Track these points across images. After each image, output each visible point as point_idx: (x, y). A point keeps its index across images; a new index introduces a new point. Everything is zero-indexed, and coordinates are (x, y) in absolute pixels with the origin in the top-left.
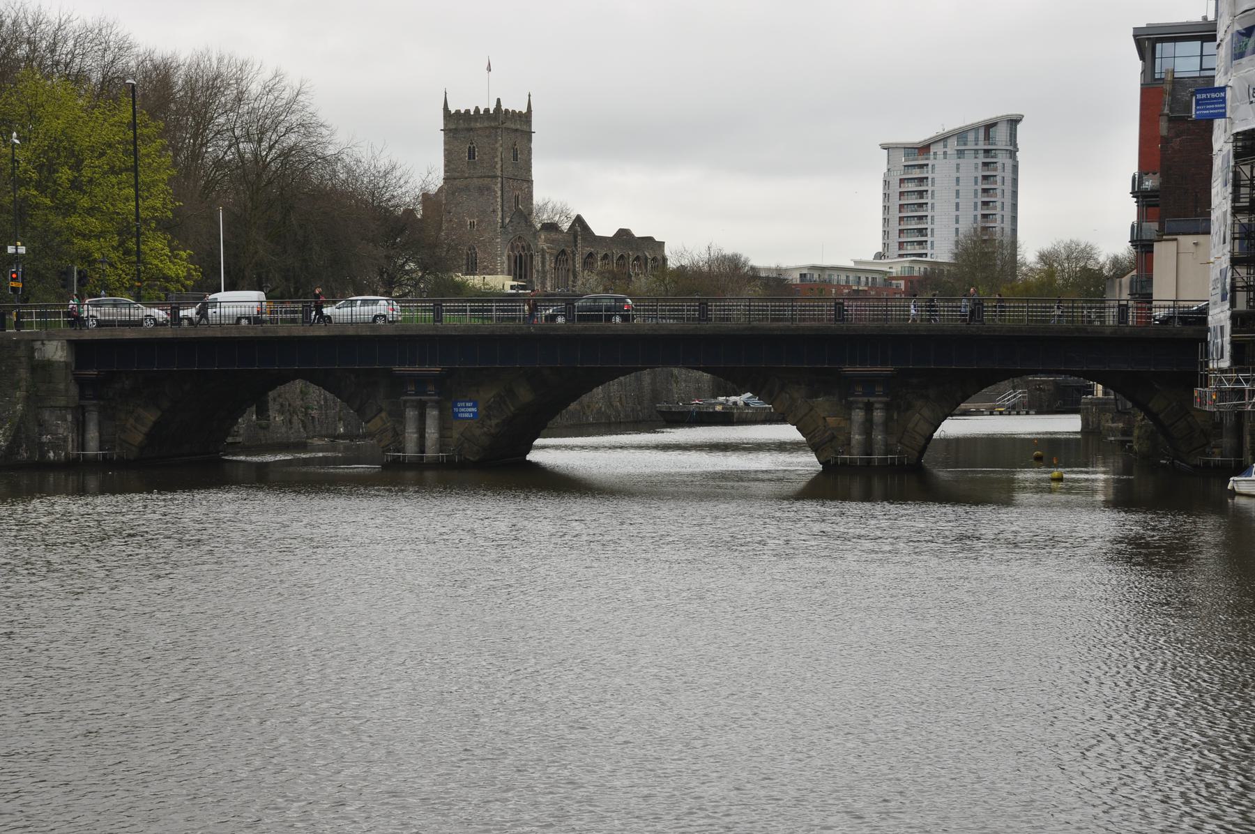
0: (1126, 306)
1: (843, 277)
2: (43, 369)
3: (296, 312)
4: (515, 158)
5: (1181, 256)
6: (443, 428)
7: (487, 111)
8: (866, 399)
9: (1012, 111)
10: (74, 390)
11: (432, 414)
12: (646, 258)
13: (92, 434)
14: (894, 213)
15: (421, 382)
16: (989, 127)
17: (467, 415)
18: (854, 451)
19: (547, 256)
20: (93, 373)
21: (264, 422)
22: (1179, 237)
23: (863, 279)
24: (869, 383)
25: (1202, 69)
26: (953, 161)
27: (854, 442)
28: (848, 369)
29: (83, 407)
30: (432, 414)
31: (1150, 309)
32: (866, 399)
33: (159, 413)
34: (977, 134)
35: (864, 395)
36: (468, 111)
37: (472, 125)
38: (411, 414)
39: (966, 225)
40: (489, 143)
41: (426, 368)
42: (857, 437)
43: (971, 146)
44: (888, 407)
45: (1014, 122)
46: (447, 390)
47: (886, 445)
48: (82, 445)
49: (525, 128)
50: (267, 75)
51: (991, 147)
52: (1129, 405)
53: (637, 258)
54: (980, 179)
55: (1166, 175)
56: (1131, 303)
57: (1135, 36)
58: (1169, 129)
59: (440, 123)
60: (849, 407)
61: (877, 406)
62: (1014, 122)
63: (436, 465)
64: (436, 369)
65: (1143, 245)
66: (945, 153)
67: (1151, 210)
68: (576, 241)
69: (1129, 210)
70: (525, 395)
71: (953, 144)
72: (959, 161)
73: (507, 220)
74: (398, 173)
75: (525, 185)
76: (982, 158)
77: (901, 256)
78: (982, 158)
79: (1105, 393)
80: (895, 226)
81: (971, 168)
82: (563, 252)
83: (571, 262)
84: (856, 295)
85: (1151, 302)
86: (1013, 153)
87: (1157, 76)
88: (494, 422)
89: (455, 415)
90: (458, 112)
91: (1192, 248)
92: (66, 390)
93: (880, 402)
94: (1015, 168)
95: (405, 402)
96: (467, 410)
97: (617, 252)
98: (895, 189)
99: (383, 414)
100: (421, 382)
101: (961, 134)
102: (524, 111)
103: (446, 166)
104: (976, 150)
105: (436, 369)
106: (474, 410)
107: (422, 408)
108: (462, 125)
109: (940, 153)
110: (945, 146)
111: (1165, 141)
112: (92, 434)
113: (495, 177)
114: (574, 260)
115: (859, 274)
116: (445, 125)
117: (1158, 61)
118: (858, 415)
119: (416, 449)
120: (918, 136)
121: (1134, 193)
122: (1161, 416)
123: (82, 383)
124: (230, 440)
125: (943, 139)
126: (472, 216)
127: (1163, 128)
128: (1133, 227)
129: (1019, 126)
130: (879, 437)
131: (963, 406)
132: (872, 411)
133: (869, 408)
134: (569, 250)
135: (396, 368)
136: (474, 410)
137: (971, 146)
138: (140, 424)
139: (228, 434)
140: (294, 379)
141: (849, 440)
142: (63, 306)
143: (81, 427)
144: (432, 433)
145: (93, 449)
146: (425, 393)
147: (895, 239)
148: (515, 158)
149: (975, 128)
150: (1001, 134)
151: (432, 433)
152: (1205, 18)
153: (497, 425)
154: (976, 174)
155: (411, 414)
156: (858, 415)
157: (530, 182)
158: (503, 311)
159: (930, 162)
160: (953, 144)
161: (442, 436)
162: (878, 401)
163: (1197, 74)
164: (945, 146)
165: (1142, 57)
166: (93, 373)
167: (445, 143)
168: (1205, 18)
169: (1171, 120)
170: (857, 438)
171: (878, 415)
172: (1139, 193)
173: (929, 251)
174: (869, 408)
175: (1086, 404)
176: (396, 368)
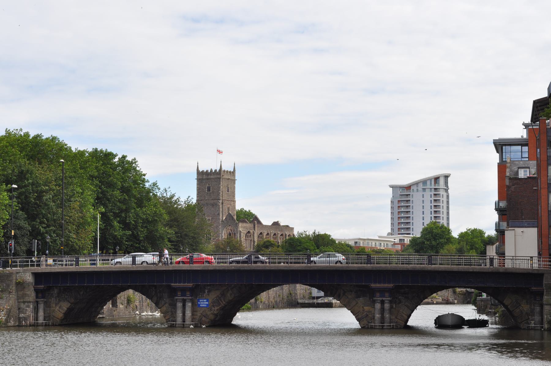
0: (493, 258)
1: (374, 243)
2: (20, 285)
4: (228, 191)
6: (193, 312)
7: (216, 171)
8: (381, 299)
9: (446, 172)
10: (33, 294)
11: (189, 305)
12: (286, 235)
13: (41, 314)
14: (396, 210)
15: (183, 291)
16: (437, 179)
17: (204, 305)
18: (376, 322)
19: (242, 234)
20: (42, 287)
21: (114, 309)
22: (516, 229)
23: (382, 244)
24: (382, 291)
26: (421, 193)
27: (376, 318)
28: (373, 285)
29: (37, 302)
30: (189, 305)
31: (504, 260)
32: (381, 299)
33: (69, 304)
35: (380, 297)
36: (207, 171)
37: (209, 177)
38: (179, 305)
39: (427, 221)
40: (213, 183)
41: (186, 284)
42: (377, 315)
43: (428, 186)
44: (391, 302)
45: (446, 177)
46: (195, 293)
47: (390, 319)
48: (36, 318)
49: (232, 178)
50: (151, 182)
51: (437, 185)
52: (497, 302)
53: (282, 235)
54: (433, 201)
55: (509, 200)
56: (497, 257)
57: (494, 143)
58: (510, 182)
59: (195, 176)
60: (374, 302)
61: (386, 302)
62: (446, 177)
63: (42, 325)
64: (190, 285)
65: (501, 232)
66: (417, 189)
67: (503, 216)
68: (254, 227)
69: (495, 217)
70: (230, 296)
71: (421, 186)
72: (424, 193)
73: (224, 218)
74: (175, 198)
75: (232, 203)
76: (433, 192)
77: (399, 234)
78: (433, 192)
79: (487, 296)
80: (396, 221)
81: (428, 196)
82: (249, 232)
83: (252, 236)
84: (379, 252)
85: (504, 257)
86: (446, 190)
87: (504, 160)
88: (216, 308)
90: (203, 171)
91: (521, 233)
92: (31, 294)
93: (388, 300)
94: (448, 197)
95: (177, 299)
96: (204, 303)
97: (272, 232)
98: (396, 205)
99: (167, 305)
100: (183, 291)
101: (424, 182)
102: (232, 170)
103: (197, 194)
104: (431, 189)
105: (190, 285)
106: (207, 303)
108: (205, 177)
109: (415, 190)
110: (417, 186)
111: (508, 187)
112: (41, 314)
113: (220, 200)
114: (254, 235)
116: (197, 177)
117: (504, 154)
118: (378, 306)
119: (181, 320)
120: (405, 181)
121: (496, 209)
122: (509, 307)
123: (37, 291)
124: (101, 316)
125: (417, 183)
126: (208, 216)
127: (507, 182)
128: (496, 224)
129: (449, 179)
130: (387, 316)
131: (426, 300)
132: (384, 304)
133: (382, 302)
134: (251, 231)
135: (173, 284)
136: (207, 303)
137: (428, 186)
138: (60, 309)
139: (99, 313)
140: (128, 289)
141: (374, 316)
142: (30, 258)
143: (36, 310)
144: (188, 313)
145: (41, 320)
146: (185, 296)
147: (396, 227)
148: (228, 191)
149: (430, 179)
150: (442, 181)
151: (188, 313)
152: (522, 136)
153: (217, 310)
154: (431, 199)
155: (179, 305)
156: (378, 306)
157: (234, 201)
158: (220, 259)
159: (411, 194)
160: (421, 186)
161: (193, 315)
162: (387, 299)
163: (520, 160)
164: (417, 186)
165: (498, 152)
166: (42, 287)
167: (198, 184)
168: (522, 136)
169: (510, 179)
170: (378, 316)
171: (387, 306)
172: (499, 210)
173: (411, 232)
174: (382, 302)
175: (479, 301)
176: (173, 284)
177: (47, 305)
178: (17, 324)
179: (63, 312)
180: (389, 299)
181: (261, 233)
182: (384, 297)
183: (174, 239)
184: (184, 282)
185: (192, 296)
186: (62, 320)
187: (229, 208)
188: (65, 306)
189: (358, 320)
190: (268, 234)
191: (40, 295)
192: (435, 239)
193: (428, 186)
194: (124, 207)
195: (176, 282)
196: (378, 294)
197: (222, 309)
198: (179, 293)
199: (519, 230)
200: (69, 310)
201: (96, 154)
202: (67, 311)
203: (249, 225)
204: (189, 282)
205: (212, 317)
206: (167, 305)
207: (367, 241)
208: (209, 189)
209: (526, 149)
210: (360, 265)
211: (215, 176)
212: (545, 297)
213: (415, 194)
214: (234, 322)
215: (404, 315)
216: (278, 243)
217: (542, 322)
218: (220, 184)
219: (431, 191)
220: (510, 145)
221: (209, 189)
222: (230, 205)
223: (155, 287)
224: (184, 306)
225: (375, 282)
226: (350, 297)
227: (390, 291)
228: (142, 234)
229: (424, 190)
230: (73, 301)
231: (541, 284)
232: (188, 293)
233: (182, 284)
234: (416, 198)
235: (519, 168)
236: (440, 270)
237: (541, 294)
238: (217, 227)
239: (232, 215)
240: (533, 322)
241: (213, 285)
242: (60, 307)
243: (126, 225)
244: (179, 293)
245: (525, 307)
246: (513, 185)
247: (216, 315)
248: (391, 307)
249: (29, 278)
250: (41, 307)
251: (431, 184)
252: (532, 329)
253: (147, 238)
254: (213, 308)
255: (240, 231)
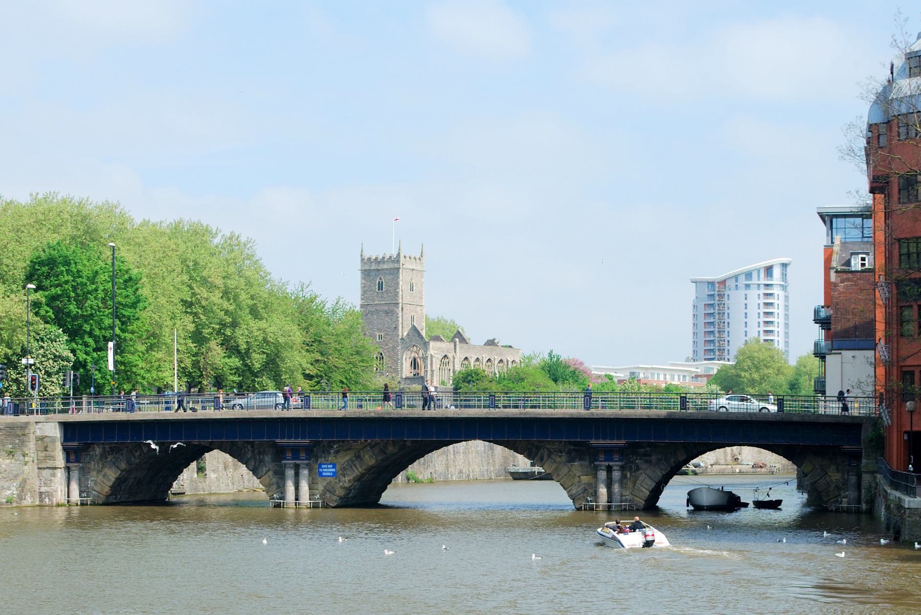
3: (409, 406)
4: (412, 289)
5: (844, 365)
8: (607, 464)
9: (785, 260)
13: (75, 487)
15: (296, 451)
16: (769, 270)
22: (843, 352)
24: (609, 452)
25: (863, 237)
32: (607, 464)
34: (759, 271)
35: (606, 460)
38: (290, 473)
41: (299, 440)
44: (622, 468)
58: (837, 277)
59: (358, 265)
60: (596, 469)
61: (615, 468)
64: (306, 441)
70: (370, 460)
73: (405, 334)
74: (318, 300)
75: (419, 308)
81: (755, 297)
88: (347, 479)
89: (320, 474)
90: (369, 259)
95: (285, 464)
96: (328, 470)
99: (270, 473)
104: (759, 285)
105: (306, 441)
106: (334, 470)
107: (297, 468)
115: (673, 373)
118: (603, 475)
123: (66, 450)
133: (609, 470)
134: (450, 356)
136: (334, 470)
146: (298, 459)
147: (702, 347)
148: (412, 289)
150: (777, 272)
153: (349, 481)
154: (759, 302)
155: (290, 473)
160: (742, 281)
162: (615, 464)
164: (737, 281)
171: (616, 475)
174: (609, 470)
177: (84, 473)
178: (37, 503)
179: (111, 484)
180: (619, 463)
181: (466, 358)
182: (612, 460)
183: (312, 371)
184: (297, 437)
185: (309, 459)
186: (108, 496)
187: (412, 318)
188: (112, 475)
189: (571, 496)
190: (478, 359)
191: (72, 457)
192: (757, 368)
193: (755, 281)
194: (229, 320)
195: (283, 438)
196: (602, 457)
197: (359, 479)
198: (289, 455)
199: (848, 354)
200: (119, 482)
201: (176, 230)
202: (115, 483)
203: (446, 346)
204: (304, 437)
205: (341, 493)
206: (270, 473)
207: (650, 371)
208: (380, 286)
209: (869, 223)
210: (522, 410)
211: (391, 266)
212: (864, 461)
213: (733, 293)
214: (381, 502)
215: (644, 490)
216: (495, 374)
217: (859, 501)
218: (398, 277)
219: (759, 289)
220: (845, 216)
221: (380, 286)
222: (416, 312)
223: (252, 444)
224: (297, 475)
225: (597, 438)
226: (558, 459)
227: (621, 451)
228: (257, 360)
229: (747, 286)
230: (123, 466)
231: (858, 441)
232: (303, 455)
233: (292, 440)
234: (735, 299)
235: (852, 254)
236: (700, 417)
237: (857, 456)
238: (394, 348)
239: (419, 329)
240: (845, 500)
241: (343, 442)
242: (104, 476)
243: (231, 348)
244: (289, 455)
245: (835, 476)
246: (842, 282)
247: (349, 489)
248: (624, 477)
249: (55, 432)
250: (75, 474)
251: (759, 276)
252: (844, 511)
253: (266, 366)
254: (343, 479)
255: (432, 356)
